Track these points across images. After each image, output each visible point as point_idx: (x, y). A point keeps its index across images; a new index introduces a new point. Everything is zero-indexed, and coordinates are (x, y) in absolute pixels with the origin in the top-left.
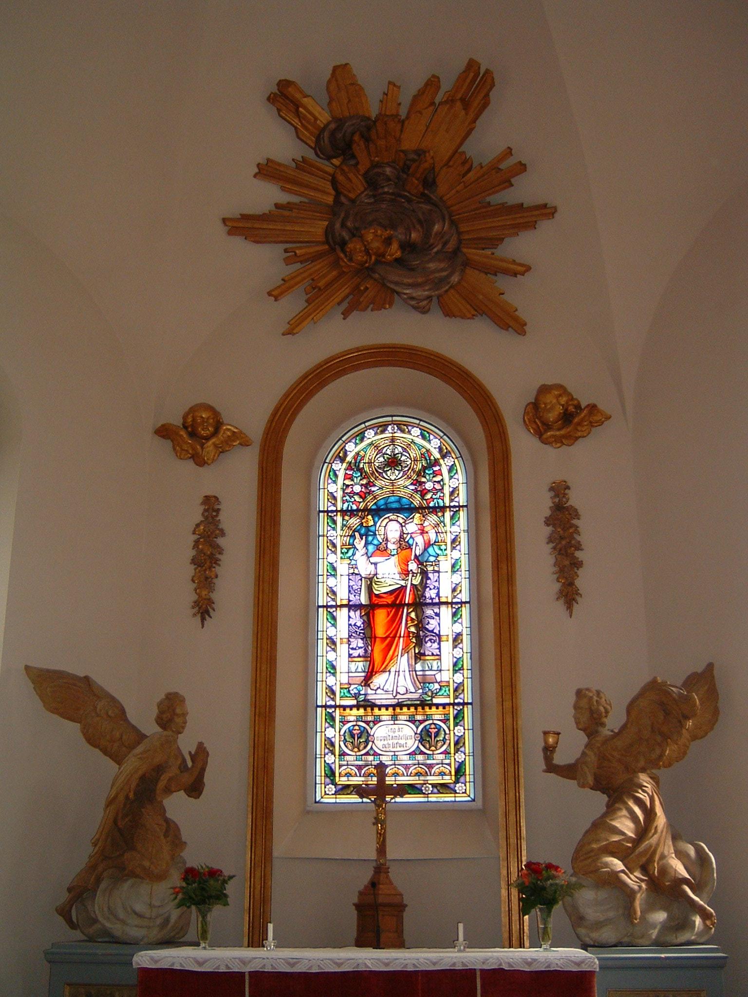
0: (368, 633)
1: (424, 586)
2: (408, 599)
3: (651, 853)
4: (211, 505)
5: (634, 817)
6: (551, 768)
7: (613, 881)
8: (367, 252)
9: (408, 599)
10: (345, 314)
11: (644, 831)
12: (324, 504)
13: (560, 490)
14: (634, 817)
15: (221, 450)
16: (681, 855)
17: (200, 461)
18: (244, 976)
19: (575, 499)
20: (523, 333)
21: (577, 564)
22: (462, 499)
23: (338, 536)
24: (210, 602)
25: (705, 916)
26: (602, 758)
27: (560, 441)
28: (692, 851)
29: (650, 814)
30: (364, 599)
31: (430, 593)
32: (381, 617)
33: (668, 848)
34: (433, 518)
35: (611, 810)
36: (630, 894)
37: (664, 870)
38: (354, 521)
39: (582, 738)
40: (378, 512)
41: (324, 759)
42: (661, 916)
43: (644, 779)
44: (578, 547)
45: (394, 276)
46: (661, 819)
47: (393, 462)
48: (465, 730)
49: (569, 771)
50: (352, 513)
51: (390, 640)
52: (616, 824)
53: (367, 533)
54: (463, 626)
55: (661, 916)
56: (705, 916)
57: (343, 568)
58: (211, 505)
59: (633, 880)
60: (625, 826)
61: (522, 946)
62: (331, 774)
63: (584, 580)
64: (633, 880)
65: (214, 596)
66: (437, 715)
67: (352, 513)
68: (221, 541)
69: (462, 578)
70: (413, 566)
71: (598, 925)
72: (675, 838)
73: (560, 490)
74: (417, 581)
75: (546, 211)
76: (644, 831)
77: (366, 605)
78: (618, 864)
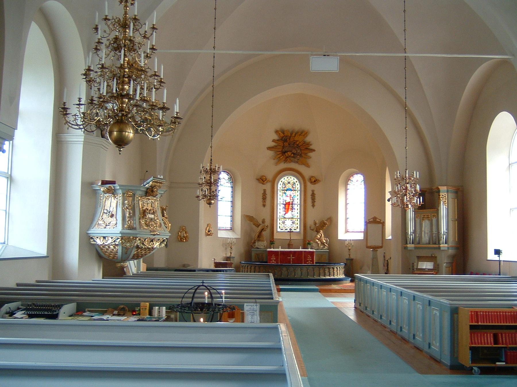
0: (285, 208)
1: (293, 202)
2: (291, 203)
3: (321, 239)
4: (265, 191)
5: (320, 235)
6: (311, 229)
7: (317, 242)
8: (288, 155)
9: (291, 203)
10: (284, 163)
11: (321, 237)
12: (279, 189)
13: (313, 191)
14: (320, 235)
15: (266, 183)
16: (325, 240)
17: (263, 184)
18: (278, 253)
19: (315, 192)
20: (309, 168)
21: (315, 202)
22: (299, 189)
23: (281, 193)
24: (265, 204)
25: (327, 246)
26: (317, 229)
27: (313, 184)
28: (326, 239)
29: (321, 235)
30: (285, 203)
31: (294, 203)
32: (287, 205)
33: (323, 239)
34: (295, 192)
35: (317, 234)
36: (318, 244)
37: (323, 241)
38: (283, 192)
39: (314, 226)
40: (286, 190)
41: (279, 225)
42: (322, 246)
43: (321, 231)
44: (315, 199)
45: (292, 159)
46: (323, 235)
47: (289, 183)
48: (298, 222)
49: (313, 230)
50: (283, 190)
51: (288, 209)
52: (318, 236)
53: (285, 193)
54: (299, 207)
55: (322, 246)
56: (327, 246)
57: (282, 198)
58: (265, 191)
59: (319, 242)
60: (319, 237)
61: (499, 321)
62: (280, 227)
63: (316, 204)
64: (319, 242)
65: (266, 204)
66: (294, 220)
67: (283, 190)
68: (266, 196)
69: (299, 201)
70: (292, 199)
71: (315, 247)
72: (324, 238)
73: (313, 191)
74: (292, 201)
75: (314, 150)
76: (321, 237)
77: (356, 297)
78: (318, 241)
